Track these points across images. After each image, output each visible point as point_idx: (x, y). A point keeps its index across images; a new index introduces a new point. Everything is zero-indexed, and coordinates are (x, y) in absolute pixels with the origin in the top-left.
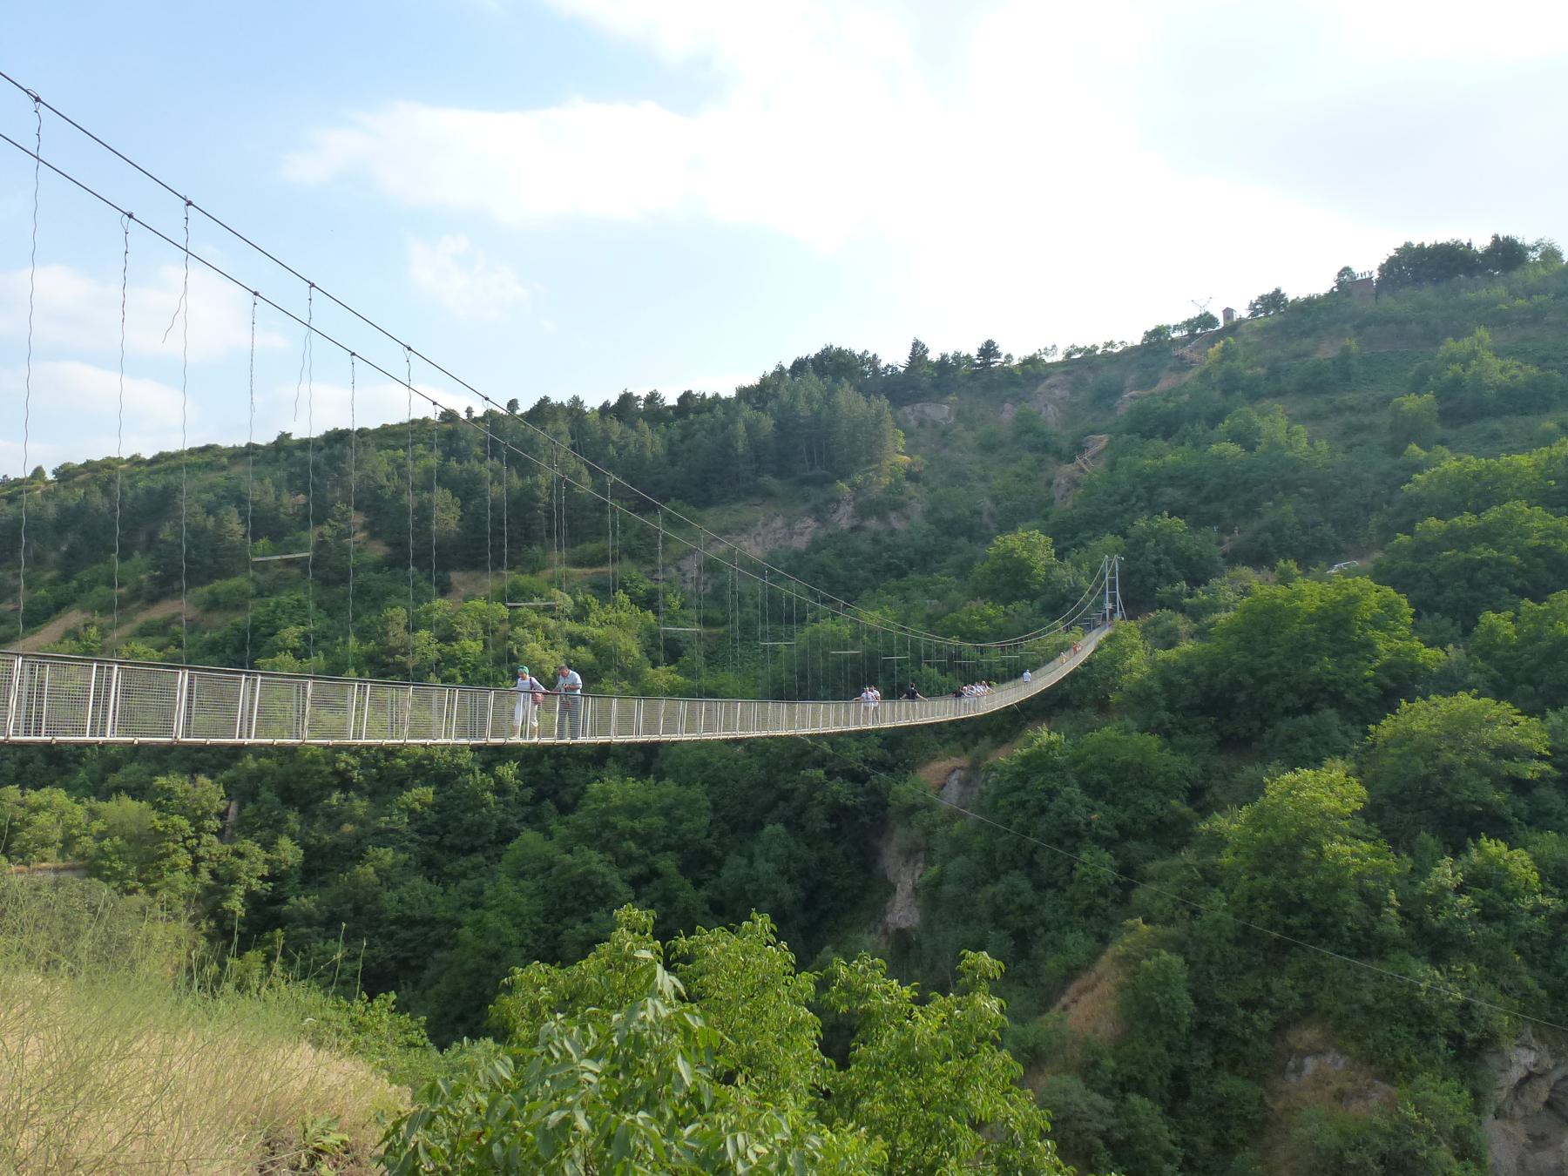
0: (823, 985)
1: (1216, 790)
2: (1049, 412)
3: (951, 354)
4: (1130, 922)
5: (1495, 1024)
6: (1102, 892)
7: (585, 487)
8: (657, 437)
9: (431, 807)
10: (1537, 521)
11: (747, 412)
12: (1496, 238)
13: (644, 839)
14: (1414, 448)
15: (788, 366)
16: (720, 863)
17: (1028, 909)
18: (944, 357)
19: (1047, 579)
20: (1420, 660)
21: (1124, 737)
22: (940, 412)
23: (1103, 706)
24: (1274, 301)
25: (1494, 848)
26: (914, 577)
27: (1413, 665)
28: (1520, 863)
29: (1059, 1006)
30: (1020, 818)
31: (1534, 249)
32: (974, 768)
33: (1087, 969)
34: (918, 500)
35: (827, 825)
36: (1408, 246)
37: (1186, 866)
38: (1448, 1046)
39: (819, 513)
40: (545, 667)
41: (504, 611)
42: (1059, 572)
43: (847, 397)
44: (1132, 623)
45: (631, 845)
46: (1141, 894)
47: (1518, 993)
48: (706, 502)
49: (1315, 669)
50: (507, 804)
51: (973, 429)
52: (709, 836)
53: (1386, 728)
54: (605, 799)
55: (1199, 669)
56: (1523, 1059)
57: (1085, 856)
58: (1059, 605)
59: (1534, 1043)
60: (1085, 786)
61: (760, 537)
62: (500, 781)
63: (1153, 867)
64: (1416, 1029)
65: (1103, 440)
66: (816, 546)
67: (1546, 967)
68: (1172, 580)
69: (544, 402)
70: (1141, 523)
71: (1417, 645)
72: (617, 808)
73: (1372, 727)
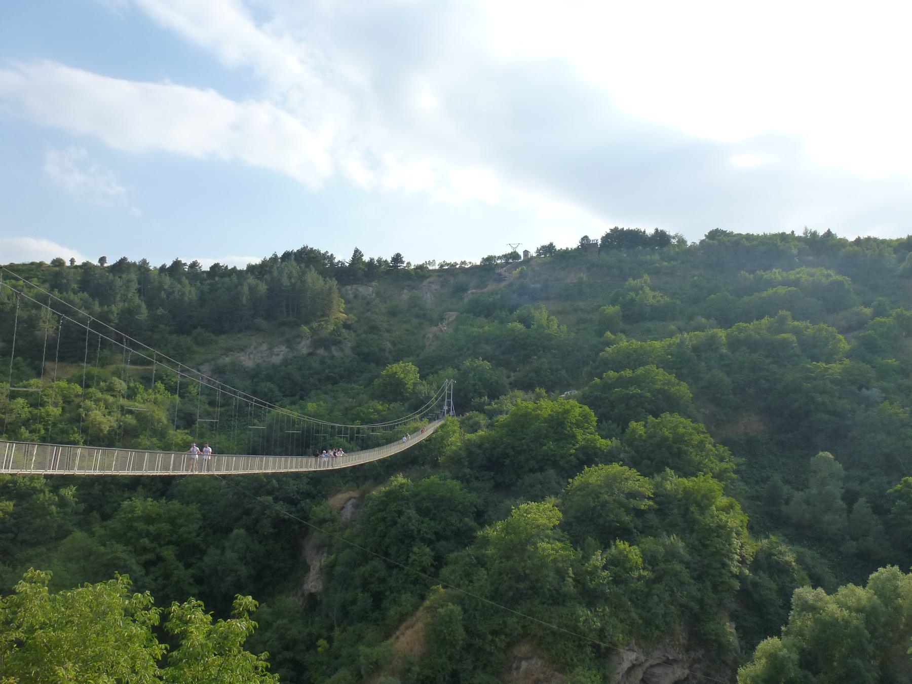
0: (164, 617)
1: (490, 513)
2: (428, 296)
3: (376, 259)
4: (434, 587)
5: (616, 639)
6: (424, 571)
7: (144, 314)
8: (193, 290)
9: (11, 515)
10: (661, 376)
11: (251, 280)
12: (657, 230)
13: (156, 538)
14: (608, 334)
15: (280, 255)
16: (203, 552)
17: (383, 580)
18: (372, 260)
19: (413, 390)
20: (598, 445)
21: (442, 482)
22: (367, 290)
23: (435, 465)
24: (549, 249)
25: (622, 545)
26: (343, 384)
27: (594, 448)
28: (634, 553)
29: (394, 636)
30: (381, 527)
31: (674, 238)
32: (362, 497)
33: (412, 615)
34: (349, 340)
35: (272, 530)
36: (616, 228)
37: (469, 555)
38: (592, 652)
39: (290, 343)
40: (103, 426)
41: (79, 389)
42: (421, 388)
43: (313, 278)
44: (455, 418)
45: (145, 541)
46: (445, 572)
47: (628, 622)
48: (220, 332)
49: (545, 448)
50: (65, 513)
51: (385, 302)
52: (198, 535)
53: (577, 480)
54: (132, 511)
55: (486, 445)
56: (629, 657)
57: (415, 549)
58: (418, 406)
59: (635, 648)
60: (419, 510)
61: (257, 353)
62: (62, 499)
63: (453, 556)
64: (577, 643)
65: (453, 316)
66: (286, 362)
67: (643, 608)
68: (481, 395)
69: (123, 261)
70: (467, 363)
71: (597, 437)
72: (139, 517)
73: (570, 480)
